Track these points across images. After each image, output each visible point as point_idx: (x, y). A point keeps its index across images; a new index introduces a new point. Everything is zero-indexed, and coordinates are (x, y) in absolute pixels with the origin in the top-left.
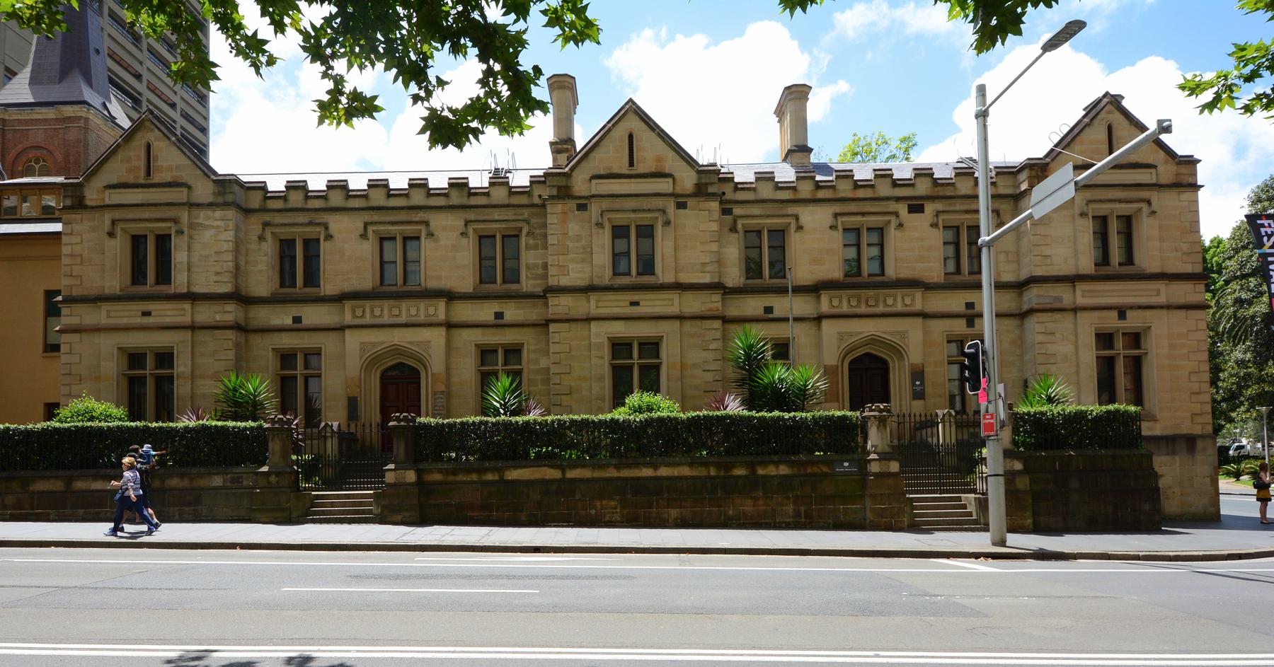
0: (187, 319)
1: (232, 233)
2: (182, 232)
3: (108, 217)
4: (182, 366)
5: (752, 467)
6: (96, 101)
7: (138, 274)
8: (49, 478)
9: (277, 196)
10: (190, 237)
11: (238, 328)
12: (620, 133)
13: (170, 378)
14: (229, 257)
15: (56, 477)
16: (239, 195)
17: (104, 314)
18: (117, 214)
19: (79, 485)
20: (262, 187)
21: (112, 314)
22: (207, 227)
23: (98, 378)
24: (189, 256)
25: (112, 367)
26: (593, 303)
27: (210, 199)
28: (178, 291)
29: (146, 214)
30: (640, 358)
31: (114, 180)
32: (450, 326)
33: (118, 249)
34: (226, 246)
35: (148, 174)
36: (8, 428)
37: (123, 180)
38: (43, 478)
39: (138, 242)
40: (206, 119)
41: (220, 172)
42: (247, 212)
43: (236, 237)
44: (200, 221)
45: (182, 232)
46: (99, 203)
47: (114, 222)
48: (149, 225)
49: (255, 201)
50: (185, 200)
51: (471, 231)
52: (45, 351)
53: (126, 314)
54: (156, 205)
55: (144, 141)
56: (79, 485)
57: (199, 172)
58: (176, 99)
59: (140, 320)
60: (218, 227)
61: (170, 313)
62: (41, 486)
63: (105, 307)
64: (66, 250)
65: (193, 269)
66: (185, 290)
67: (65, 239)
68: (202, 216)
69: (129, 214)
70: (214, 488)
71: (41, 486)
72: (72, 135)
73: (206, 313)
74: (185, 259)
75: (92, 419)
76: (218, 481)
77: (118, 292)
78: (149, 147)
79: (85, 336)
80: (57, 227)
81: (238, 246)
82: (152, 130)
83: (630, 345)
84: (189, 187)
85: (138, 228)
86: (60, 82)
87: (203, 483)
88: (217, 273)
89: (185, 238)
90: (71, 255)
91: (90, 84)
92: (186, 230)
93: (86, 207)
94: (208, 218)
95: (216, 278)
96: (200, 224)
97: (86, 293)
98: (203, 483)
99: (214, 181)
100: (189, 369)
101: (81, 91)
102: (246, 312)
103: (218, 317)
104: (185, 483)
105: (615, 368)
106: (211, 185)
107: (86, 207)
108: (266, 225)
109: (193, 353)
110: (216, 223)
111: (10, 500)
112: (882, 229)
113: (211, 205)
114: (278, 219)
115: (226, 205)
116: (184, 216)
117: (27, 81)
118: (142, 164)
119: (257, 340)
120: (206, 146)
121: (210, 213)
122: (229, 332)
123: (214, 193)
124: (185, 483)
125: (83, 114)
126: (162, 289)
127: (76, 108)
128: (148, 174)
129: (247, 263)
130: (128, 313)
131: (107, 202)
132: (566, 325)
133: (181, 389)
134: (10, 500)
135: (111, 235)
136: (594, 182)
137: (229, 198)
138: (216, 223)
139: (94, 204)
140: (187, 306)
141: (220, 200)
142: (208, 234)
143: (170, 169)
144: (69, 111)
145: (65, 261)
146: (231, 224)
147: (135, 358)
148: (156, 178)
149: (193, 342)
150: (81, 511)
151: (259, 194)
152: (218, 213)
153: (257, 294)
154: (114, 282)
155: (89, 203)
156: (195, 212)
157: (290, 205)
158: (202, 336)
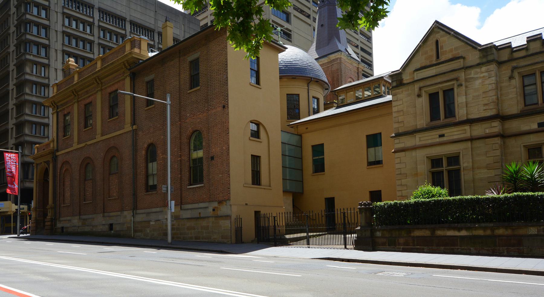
0: (468, 135)
1: (494, 78)
2: (461, 85)
3: (417, 86)
4: (465, 163)
5: (493, 230)
6: (343, 49)
7: (434, 114)
8: (421, 229)
9: (520, 49)
10: (466, 87)
11: (503, 136)
12: (432, 41)
13: (458, 171)
14: (492, 93)
15: (426, 229)
16: (495, 55)
17: (417, 139)
18: (422, 84)
19: (439, 233)
20: (508, 46)
21: (422, 139)
22: (477, 79)
23: (416, 175)
24: (466, 98)
25: (424, 168)
26: (417, 139)
27: (478, 61)
28: (460, 120)
29: (438, 80)
30: (448, 165)
31: (418, 66)
32: (503, 136)
33: (424, 102)
34: (490, 87)
35: (438, 57)
36: (396, 203)
37: (423, 65)
38: (418, 229)
39: (433, 98)
40: (371, 48)
41: (482, 44)
42: (500, 64)
43: (496, 80)
44: (472, 76)
45: (461, 85)
46: (411, 81)
47: (420, 89)
48: (440, 86)
49: (505, 56)
50: (462, 66)
51: (516, 74)
52: (368, 166)
53: (430, 138)
54: (444, 73)
55: (434, 40)
56: (439, 233)
57: (469, 48)
58: (358, 43)
59: (438, 140)
60: (484, 77)
61: (456, 133)
62: (417, 233)
63: (418, 136)
64: (394, 109)
65: (468, 106)
66: (465, 118)
67: (394, 104)
68: (473, 73)
69: (428, 82)
70: (531, 236)
71: (417, 233)
72: (335, 67)
73: (478, 130)
74: (464, 100)
75: (433, 196)
76: (533, 231)
77: (425, 127)
78: (437, 42)
79: (408, 153)
80: (389, 98)
81: (498, 87)
82: (439, 32)
83: (442, 159)
84: (464, 58)
85: (432, 90)
86: (328, 44)
87: (522, 232)
88: (485, 105)
89: (463, 88)
90: (398, 112)
91: (340, 42)
92: (463, 83)
93: (404, 84)
94: (477, 73)
95: (485, 108)
96: (472, 78)
97: (407, 130)
98: (522, 232)
99: (480, 50)
100: (471, 164)
101: (337, 46)
102: (503, 126)
103: (487, 131)
104: (509, 232)
105: (433, 173)
106: (478, 52)
107: (404, 84)
108: (514, 68)
109: (472, 154)
110: (482, 75)
111: (402, 241)
112: (523, 76)
113: (479, 65)
114: (522, 63)
115: (489, 62)
116: (462, 75)
117: (315, 49)
118: (434, 53)
119: (511, 142)
120: (372, 62)
121: (478, 70)
122: (496, 139)
123: (480, 58)
124: (509, 232)
125: (339, 56)
126: (450, 120)
127: (336, 54)
128: (438, 57)
129: (501, 95)
130: (432, 137)
131: (416, 79)
132: (403, 153)
133: (465, 176)
134: (402, 241)
135: (419, 96)
136: (415, 73)
137: (490, 58)
138: (482, 75)
139: (408, 82)
140: (467, 127)
141: (484, 60)
142: (478, 82)
143: (451, 51)
144: (333, 57)
145: (394, 115)
146: (493, 73)
147: (436, 162)
148: (443, 58)
149: (472, 148)
150: (442, 248)
151: (508, 50)
152: (484, 69)
153: (510, 113)
154: (423, 121)
155: (405, 82)
156: (468, 71)
157: (530, 52)
158: (477, 144)
